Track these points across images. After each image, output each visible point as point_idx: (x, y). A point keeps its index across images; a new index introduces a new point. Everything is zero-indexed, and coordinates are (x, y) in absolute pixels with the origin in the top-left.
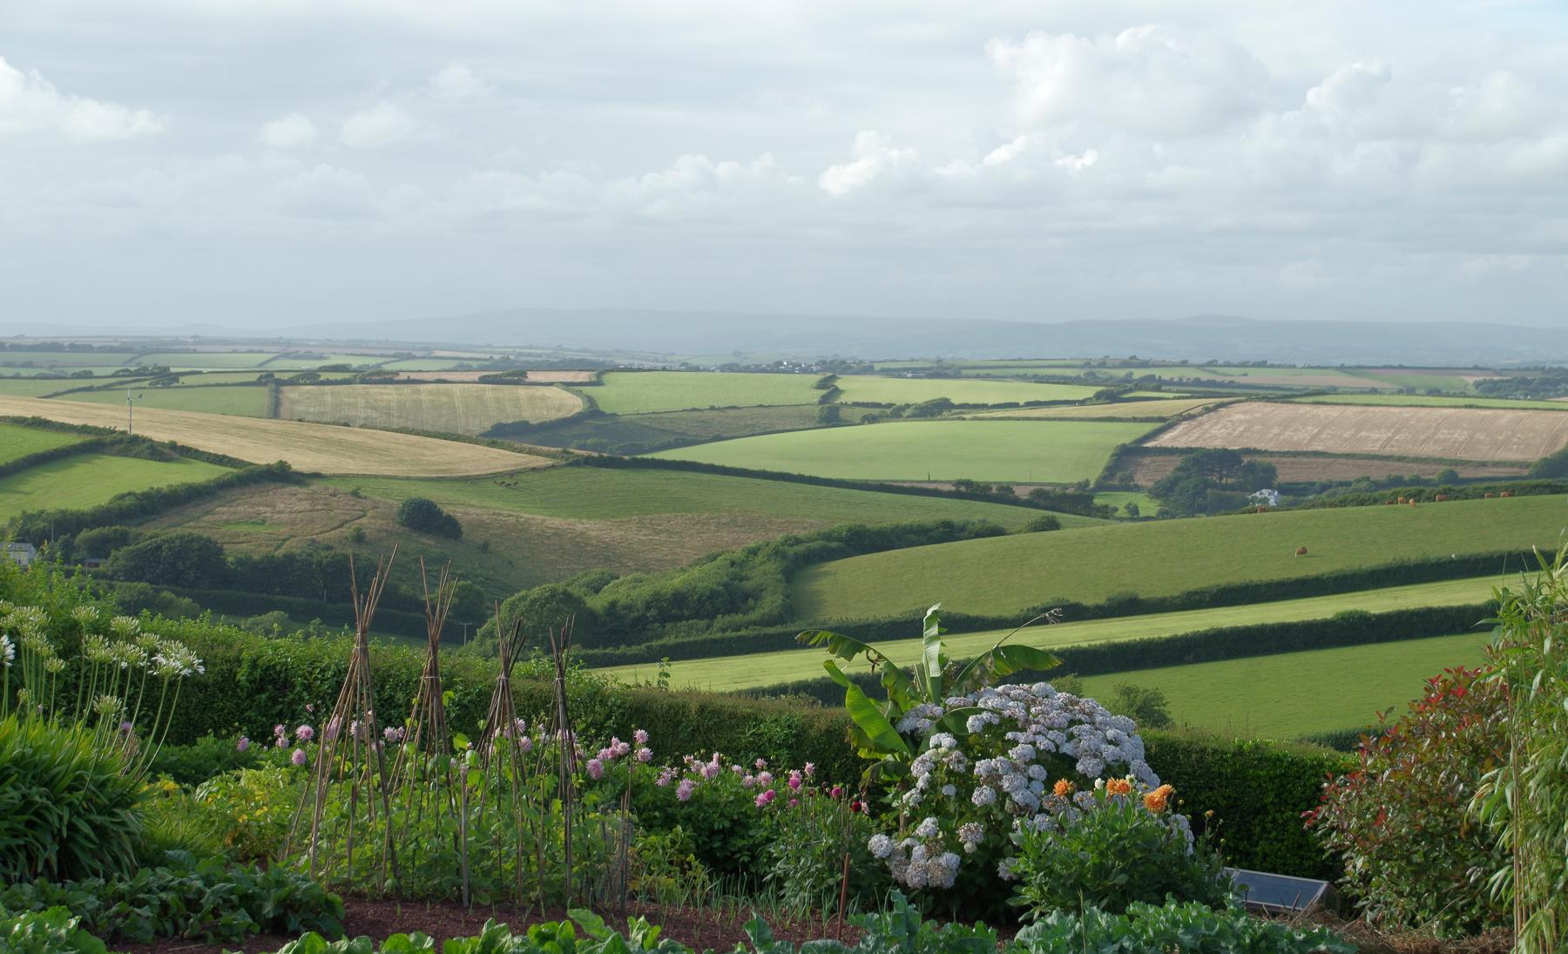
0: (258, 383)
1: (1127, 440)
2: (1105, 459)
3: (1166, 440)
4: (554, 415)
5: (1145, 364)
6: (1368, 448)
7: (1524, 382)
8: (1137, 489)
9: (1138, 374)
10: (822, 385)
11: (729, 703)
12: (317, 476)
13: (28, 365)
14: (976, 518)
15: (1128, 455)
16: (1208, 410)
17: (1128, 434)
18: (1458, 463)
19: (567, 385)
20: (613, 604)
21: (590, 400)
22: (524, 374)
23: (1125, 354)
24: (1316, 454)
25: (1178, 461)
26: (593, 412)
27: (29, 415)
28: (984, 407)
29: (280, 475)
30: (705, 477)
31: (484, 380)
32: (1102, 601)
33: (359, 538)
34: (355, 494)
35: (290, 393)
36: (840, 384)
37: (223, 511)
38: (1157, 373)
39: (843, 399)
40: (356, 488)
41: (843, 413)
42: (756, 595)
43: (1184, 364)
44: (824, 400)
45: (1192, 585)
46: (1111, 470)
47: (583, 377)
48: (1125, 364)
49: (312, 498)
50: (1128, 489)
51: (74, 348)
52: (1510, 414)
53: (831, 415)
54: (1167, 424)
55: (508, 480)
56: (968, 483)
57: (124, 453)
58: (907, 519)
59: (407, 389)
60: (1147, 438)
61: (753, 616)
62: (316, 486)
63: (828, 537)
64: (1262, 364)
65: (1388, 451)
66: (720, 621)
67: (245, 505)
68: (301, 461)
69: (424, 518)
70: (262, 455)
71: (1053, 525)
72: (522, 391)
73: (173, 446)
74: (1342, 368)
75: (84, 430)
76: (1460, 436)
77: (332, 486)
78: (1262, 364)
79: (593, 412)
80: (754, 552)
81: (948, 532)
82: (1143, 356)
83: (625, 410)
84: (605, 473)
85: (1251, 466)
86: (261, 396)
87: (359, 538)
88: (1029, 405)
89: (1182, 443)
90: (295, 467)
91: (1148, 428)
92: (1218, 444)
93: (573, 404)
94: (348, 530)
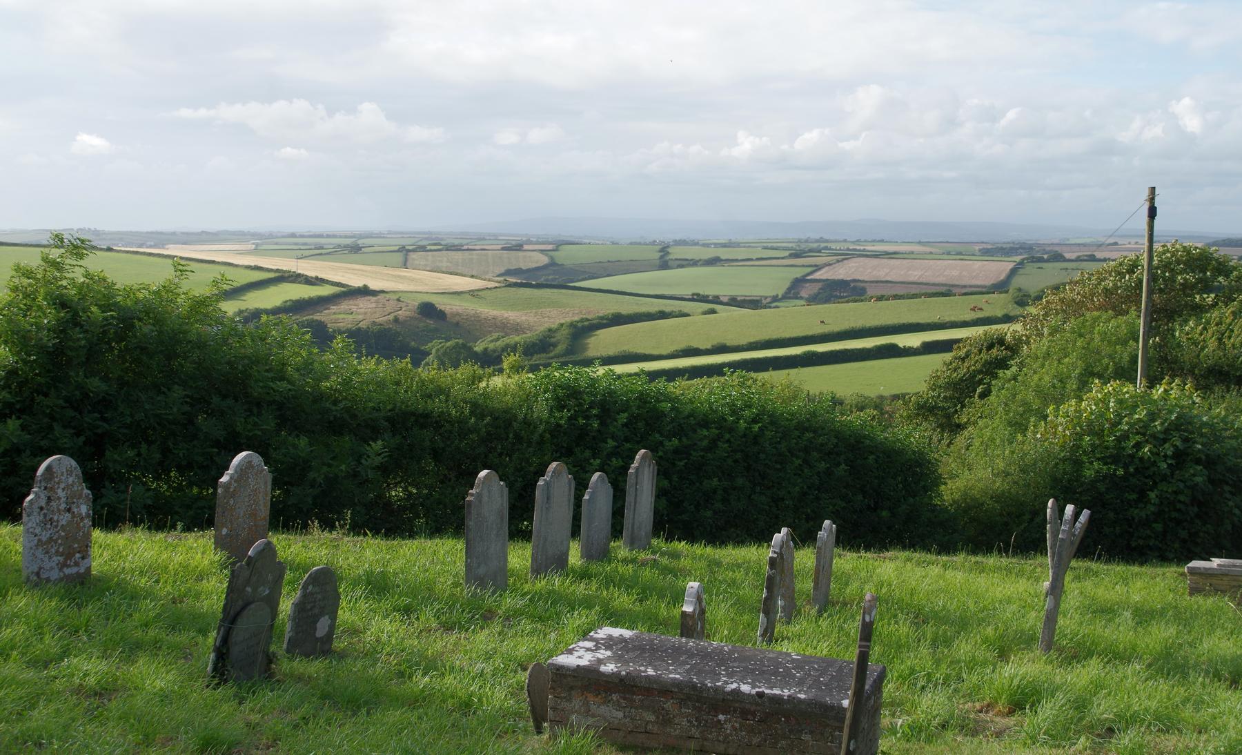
0: (398, 251)
1: (798, 276)
2: (788, 284)
3: (817, 275)
4: (534, 265)
5: (827, 241)
6: (911, 279)
7: (1002, 249)
8: (801, 298)
9: (823, 245)
10: (661, 251)
11: (855, 419)
12: (383, 292)
13: (305, 244)
14: (676, 309)
15: (798, 283)
16: (838, 261)
17: (798, 273)
18: (953, 286)
19: (542, 251)
20: (486, 349)
21: (552, 258)
22: (521, 246)
23: (818, 237)
24: (887, 282)
25: (820, 285)
26: (553, 264)
27: (252, 264)
28: (737, 260)
29: (365, 292)
30: (577, 292)
31: (503, 249)
32: (709, 347)
33: (396, 320)
34: (398, 300)
35: (413, 256)
36: (669, 250)
37: (334, 308)
38: (829, 245)
39: (671, 257)
40: (399, 297)
41: (670, 263)
42: (555, 345)
43: (845, 241)
44: (662, 257)
45: (757, 338)
46: (789, 289)
47: (550, 247)
48: (817, 241)
49: (377, 302)
50: (797, 298)
51: (328, 236)
52: (980, 263)
53: (664, 265)
54: (818, 268)
55: (473, 293)
56: (698, 295)
57: (293, 282)
58: (643, 309)
59: (467, 253)
60: (809, 274)
61: (552, 354)
62: (381, 296)
63: (602, 318)
64: (882, 241)
65: (921, 280)
66: (536, 357)
67: (345, 305)
68: (374, 285)
69: (428, 310)
70: (356, 282)
71: (713, 312)
72: (520, 254)
73: (317, 278)
74: (920, 243)
75: (277, 271)
76: (955, 273)
77: (388, 296)
78: (882, 241)
79: (553, 264)
80: (562, 325)
81: (662, 315)
82: (826, 237)
83: (568, 263)
84: (523, 290)
85: (855, 288)
86: (399, 257)
87: (396, 320)
88: (758, 259)
89: (824, 277)
90: (901, 345)
91: (809, 270)
92: (841, 277)
93: (544, 260)
94: (391, 317)
